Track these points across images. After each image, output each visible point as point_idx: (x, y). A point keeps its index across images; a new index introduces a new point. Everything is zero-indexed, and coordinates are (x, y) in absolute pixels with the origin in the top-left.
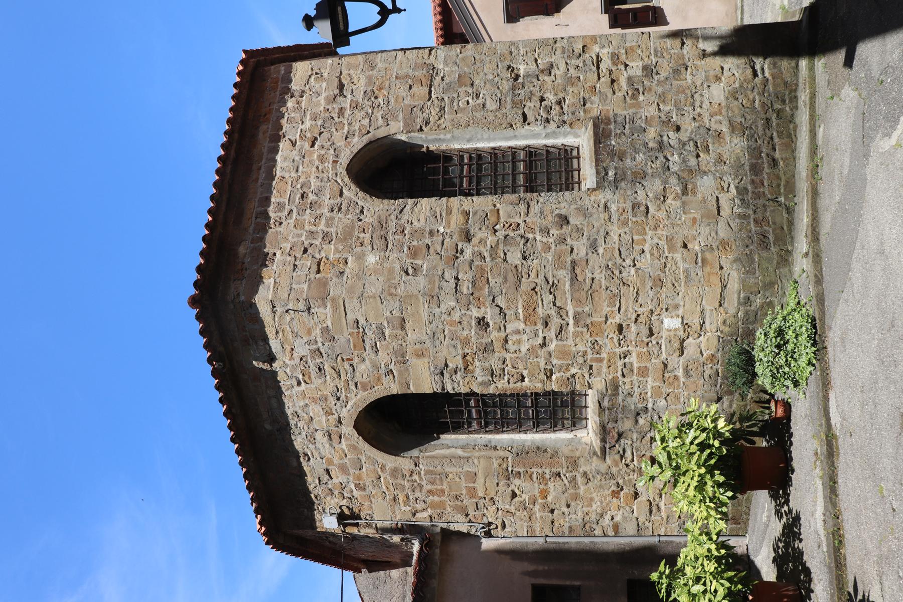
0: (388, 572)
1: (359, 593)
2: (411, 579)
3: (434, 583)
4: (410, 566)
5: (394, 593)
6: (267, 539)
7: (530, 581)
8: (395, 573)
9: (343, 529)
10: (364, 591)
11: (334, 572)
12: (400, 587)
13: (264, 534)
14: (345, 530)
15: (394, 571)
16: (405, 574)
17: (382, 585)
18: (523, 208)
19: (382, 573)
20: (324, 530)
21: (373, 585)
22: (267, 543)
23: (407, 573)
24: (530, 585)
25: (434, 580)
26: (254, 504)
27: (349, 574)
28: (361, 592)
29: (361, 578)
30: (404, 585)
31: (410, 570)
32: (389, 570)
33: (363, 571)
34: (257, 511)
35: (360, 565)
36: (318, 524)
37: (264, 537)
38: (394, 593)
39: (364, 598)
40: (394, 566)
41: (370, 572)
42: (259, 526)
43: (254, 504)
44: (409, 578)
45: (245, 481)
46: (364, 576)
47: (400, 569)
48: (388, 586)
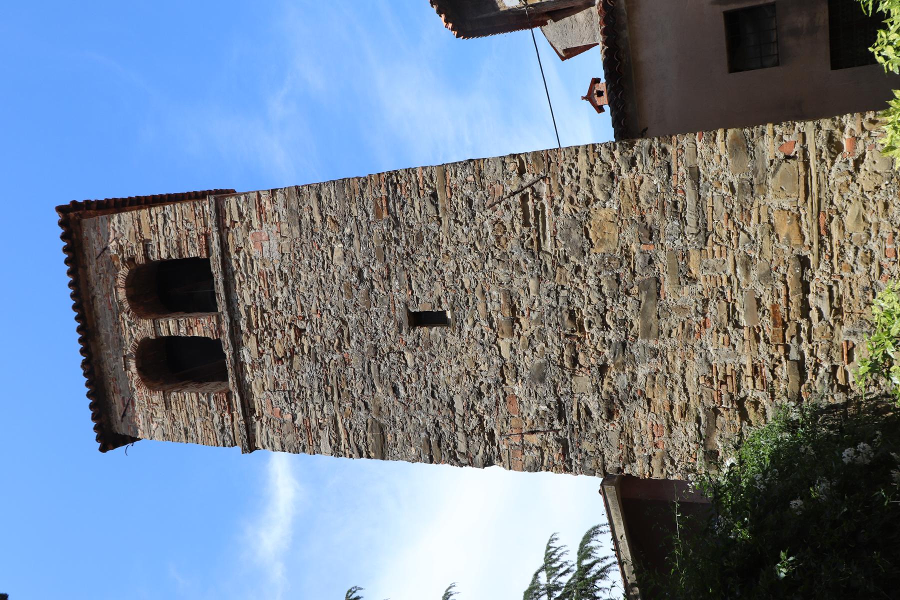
0: (573, 17)
1: (550, 43)
2: (597, 19)
3: (625, 34)
4: (594, 5)
5: (583, 36)
6: (456, 32)
7: (721, 9)
8: (580, 16)
9: (524, 3)
10: (554, 40)
11: (524, 35)
12: (588, 28)
13: (452, 29)
14: (527, 3)
15: (578, 14)
16: (590, 14)
17: (570, 31)
18: (695, 231)
19: (567, 19)
20: (506, 9)
21: (562, 32)
22: (458, 36)
23: (591, 13)
24: (722, 14)
25: (624, 31)
26: (435, 6)
27: (537, 30)
28: (552, 42)
29: (549, 29)
30: (592, 25)
31: (594, 10)
32: (574, 14)
33: (548, 22)
34: (439, 12)
35: (544, 18)
36: (499, 5)
37: (453, 32)
38: (583, 36)
39: (556, 46)
40: (578, 9)
41: (555, 21)
42: (445, 24)
43: (442, 15)
44: (595, 18)
45: (440, 16)
46: (551, 25)
47: (585, 11)
48: (576, 30)
